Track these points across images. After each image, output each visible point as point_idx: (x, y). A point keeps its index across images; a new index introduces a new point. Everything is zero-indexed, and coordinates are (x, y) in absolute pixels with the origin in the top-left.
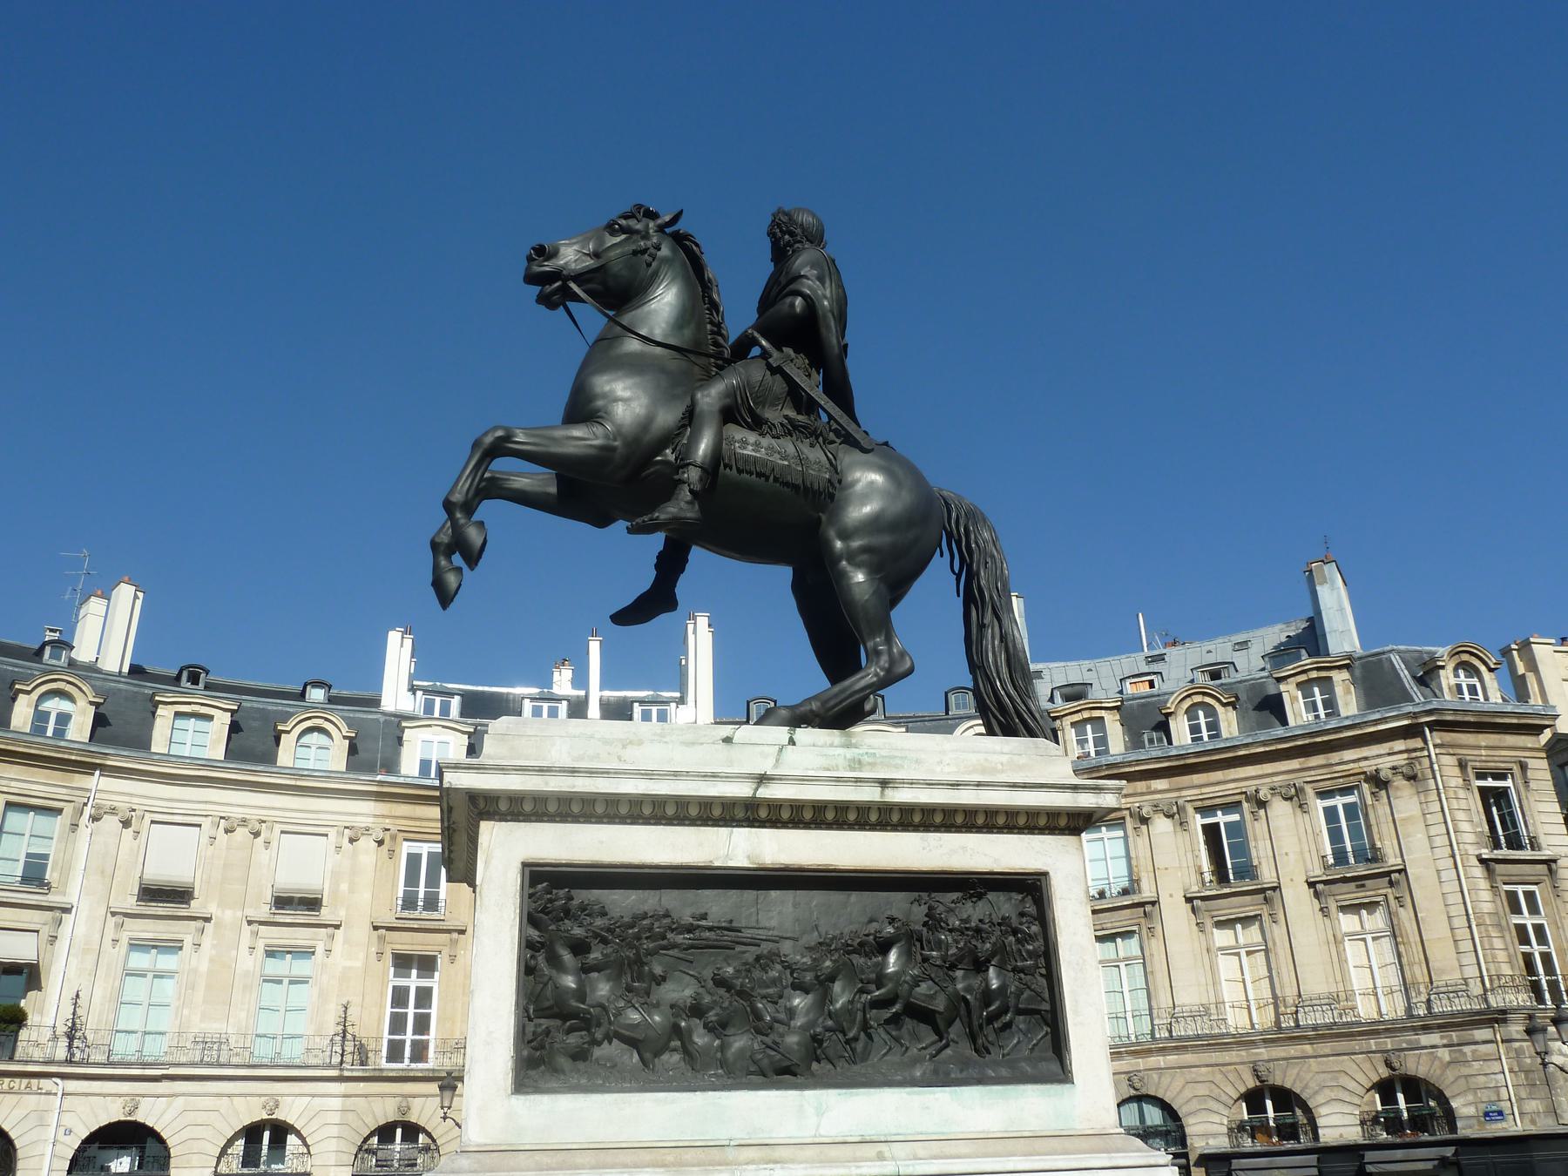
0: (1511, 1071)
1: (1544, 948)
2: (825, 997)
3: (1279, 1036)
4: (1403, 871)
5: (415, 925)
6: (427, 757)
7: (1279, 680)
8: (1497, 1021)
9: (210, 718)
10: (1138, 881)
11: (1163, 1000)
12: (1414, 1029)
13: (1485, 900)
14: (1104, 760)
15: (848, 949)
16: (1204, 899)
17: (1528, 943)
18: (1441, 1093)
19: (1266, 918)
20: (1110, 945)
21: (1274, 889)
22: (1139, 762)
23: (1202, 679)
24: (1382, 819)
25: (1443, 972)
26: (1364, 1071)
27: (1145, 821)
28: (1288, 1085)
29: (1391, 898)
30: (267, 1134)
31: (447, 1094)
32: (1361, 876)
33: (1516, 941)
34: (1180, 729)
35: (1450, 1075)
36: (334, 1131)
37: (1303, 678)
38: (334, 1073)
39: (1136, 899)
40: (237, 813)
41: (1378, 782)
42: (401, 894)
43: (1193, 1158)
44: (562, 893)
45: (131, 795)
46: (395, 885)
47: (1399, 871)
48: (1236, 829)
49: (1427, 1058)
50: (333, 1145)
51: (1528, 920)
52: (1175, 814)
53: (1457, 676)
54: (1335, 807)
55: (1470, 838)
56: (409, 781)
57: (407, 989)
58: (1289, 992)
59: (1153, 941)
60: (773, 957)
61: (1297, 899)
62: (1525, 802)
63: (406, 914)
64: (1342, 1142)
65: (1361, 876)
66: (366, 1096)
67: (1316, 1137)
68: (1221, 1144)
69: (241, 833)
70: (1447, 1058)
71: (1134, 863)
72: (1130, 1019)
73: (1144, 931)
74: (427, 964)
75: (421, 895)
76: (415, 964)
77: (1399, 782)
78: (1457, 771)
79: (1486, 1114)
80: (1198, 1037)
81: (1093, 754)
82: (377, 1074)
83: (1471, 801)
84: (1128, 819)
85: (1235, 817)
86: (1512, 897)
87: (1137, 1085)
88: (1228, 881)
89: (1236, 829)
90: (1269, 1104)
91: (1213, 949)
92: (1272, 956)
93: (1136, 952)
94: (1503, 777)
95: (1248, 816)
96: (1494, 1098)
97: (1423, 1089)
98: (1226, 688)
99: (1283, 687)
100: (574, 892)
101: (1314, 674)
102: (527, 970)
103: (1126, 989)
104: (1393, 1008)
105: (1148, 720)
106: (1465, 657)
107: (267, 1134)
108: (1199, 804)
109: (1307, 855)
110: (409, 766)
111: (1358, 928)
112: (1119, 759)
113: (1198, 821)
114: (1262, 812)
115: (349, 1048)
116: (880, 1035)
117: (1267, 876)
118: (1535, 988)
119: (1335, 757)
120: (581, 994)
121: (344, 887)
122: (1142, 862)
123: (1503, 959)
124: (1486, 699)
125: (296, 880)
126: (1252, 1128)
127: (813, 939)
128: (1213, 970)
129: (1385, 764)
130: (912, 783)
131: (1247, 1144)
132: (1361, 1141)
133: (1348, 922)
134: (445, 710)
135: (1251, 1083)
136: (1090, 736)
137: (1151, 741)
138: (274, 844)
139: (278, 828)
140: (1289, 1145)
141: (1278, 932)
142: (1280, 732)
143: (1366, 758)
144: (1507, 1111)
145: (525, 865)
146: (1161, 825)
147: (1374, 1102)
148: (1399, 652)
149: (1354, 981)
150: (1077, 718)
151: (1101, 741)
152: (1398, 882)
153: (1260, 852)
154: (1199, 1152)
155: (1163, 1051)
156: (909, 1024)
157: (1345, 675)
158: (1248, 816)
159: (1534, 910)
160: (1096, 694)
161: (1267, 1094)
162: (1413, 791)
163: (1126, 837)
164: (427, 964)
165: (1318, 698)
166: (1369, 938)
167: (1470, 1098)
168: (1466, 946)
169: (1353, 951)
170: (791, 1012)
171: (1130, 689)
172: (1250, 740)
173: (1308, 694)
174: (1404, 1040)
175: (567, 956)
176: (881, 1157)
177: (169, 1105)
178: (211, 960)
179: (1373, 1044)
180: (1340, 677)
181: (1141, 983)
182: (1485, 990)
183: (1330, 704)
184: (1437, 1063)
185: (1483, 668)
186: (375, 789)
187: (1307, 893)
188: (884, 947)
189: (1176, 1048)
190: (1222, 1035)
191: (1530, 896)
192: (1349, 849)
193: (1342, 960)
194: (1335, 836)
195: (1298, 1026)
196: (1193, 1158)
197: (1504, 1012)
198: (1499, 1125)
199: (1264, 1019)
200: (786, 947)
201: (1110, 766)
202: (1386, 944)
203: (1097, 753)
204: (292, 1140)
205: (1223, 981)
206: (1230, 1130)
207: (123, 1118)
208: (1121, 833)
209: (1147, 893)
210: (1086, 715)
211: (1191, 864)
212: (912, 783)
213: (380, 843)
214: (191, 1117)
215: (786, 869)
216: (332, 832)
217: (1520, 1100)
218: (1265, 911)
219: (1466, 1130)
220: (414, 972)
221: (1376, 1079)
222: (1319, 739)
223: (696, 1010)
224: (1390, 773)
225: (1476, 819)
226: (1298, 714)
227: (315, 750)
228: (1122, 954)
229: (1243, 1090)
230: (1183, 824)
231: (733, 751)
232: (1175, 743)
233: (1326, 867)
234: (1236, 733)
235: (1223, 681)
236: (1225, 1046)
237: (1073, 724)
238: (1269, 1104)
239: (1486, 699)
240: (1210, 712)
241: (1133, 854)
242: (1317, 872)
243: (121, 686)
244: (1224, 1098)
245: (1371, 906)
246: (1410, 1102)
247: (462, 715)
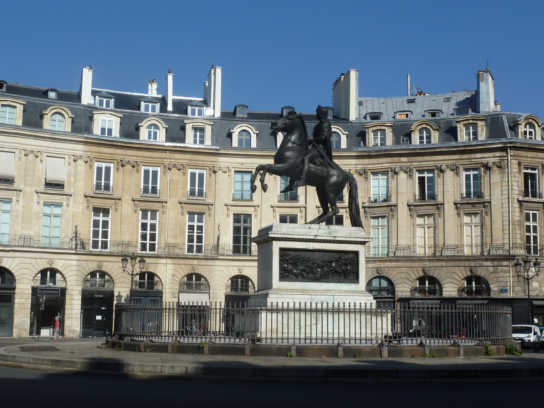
0: (513, 276)
1: (535, 234)
2: (323, 269)
3: (434, 258)
4: (490, 202)
5: (101, 196)
6: (103, 127)
7: (458, 122)
8: (512, 259)
9: (15, 107)
10: (390, 197)
11: (394, 242)
12: (482, 260)
13: (517, 215)
14: (383, 148)
15: (327, 262)
16: (414, 206)
17: (530, 232)
18: (487, 282)
19: (436, 215)
20: (377, 220)
21: (441, 204)
22: (397, 150)
23: (428, 117)
24: (486, 182)
25: (497, 240)
26: (462, 273)
27: (396, 173)
28: (434, 276)
29: (484, 212)
30: (49, 273)
31: (125, 262)
32: (475, 202)
33: (525, 231)
34: (416, 138)
35: (492, 276)
36: (74, 273)
37: (466, 122)
38: (74, 252)
39: (389, 203)
40: (29, 148)
41: (487, 167)
42: (95, 184)
43: (396, 299)
46: (92, 180)
47: (488, 202)
48: (431, 180)
49: (485, 270)
50: (74, 278)
51: (531, 224)
52: (409, 172)
53: (525, 127)
54: (470, 175)
55: (516, 192)
56: (98, 137)
57: (99, 221)
58: (441, 243)
59: (393, 220)
60: (316, 263)
61: (449, 209)
62: (540, 180)
63: (97, 192)
64: (450, 296)
65: (475, 202)
66: (86, 261)
67: (441, 294)
68: (407, 295)
69: (31, 156)
70: (492, 270)
71: (390, 189)
72: (380, 249)
73: (390, 216)
74: (106, 212)
75: (103, 184)
76: (102, 211)
77: (495, 168)
78: (517, 166)
79: (501, 290)
80: (404, 257)
81: (379, 145)
82: (90, 253)
83: (520, 177)
84: (390, 172)
85: (431, 175)
86: (528, 215)
87: (380, 272)
88: (425, 199)
89: (431, 180)
90: (427, 282)
91: (415, 225)
92: (437, 229)
93: (386, 224)
94: (535, 169)
95: (436, 175)
96: (505, 285)
97: (482, 280)
98: (436, 122)
99: (458, 125)
101: (471, 121)
102: (280, 264)
103: (380, 237)
104: (476, 251)
105: (403, 132)
106: (530, 121)
107: (49, 273)
108: (418, 169)
109: (456, 192)
110: (97, 131)
111: (470, 222)
112: (389, 148)
113: (417, 175)
114: (442, 174)
115: (79, 242)
116: (331, 275)
117: (440, 199)
118: (528, 249)
119: (473, 156)
120: (287, 267)
121: (73, 180)
122: (393, 189)
123: (519, 238)
124: (535, 138)
125: (52, 177)
126: (420, 290)
127: (321, 260)
128: (414, 233)
129: (491, 161)
131: (417, 295)
132: (457, 297)
133: (467, 219)
134: (108, 104)
135: (422, 274)
136: (379, 137)
137: (403, 141)
138: (44, 161)
139: (45, 154)
140: (432, 297)
141: (440, 220)
142: (454, 144)
143: (484, 158)
144: (508, 290)
146: (403, 176)
147: (464, 284)
148: (506, 114)
149: (465, 241)
150: (374, 129)
151: (383, 139)
152: (487, 206)
153: (438, 190)
154: (399, 297)
155: (391, 261)
156: (335, 274)
157: (483, 123)
158: (436, 175)
159: (535, 220)
160: (384, 118)
161: (427, 279)
162: (499, 172)
163: (388, 179)
164: (106, 212)
165: (471, 131)
166: (473, 226)
167: (497, 284)
168: (506, 232)
169: (466, 230)
170: (318, 271)
171: (398, 117)
172: (442, 146)
173: (467, 129)
174: (478, 263)
175: (286, 262)
177: (13, 261)
179: (467, 264)
180: (480, 124)
181: (386, 236)
182: (510, 248)
183: (475, 134)
184: (488, 272)
185: (536, 125)
186: (84, 140)
187: (453, 206)
188: (332, 262)
189: (396, 260)
190: (413, 257)
191: (534, 215)
192: (472, 192)
193: (462, 233)
194: (468, 186)
195: (441, 255)
196: (396, 299)
197: (514, 256)
198: (505, 294)
199: (429, 252)
200: (317, 261)
201: (385, 150)
202: (479, 228)
203: (381, 144)
204: (58, 276)
205: (416, 237)
206: (411, 290)
208: (386, 177)
209: (393, 201)
210: (378, 128)
211: (412, 192)
213: (86, 162)
214: (22, 266)
216: (67, 157)
217: (513, 286)
218: (437, 212)
219: (493, 295)
220: (101, 214)
221: (466, 276)
222: (468, 148)
223: (304, 270)
224: (492, 164)
225: (520, 185)
226: (463, 136)
227: (57, 121)
228: (380, 224)
229: (418, 276)
230: (411, 176)
231: (311, 230)
232: (413, 143)
233: (462, 198)
234: (437, 142)
235: (436, 118)
236: (414, 261)
237: (373, 131)
238: (427, 282)
239: (535, 138)
240: (428, 131)
241: (390, 186)
242: (459, 199)
244: (411, 279)
245: (476, 214)
246: (477, 285)
247: (115, 107)
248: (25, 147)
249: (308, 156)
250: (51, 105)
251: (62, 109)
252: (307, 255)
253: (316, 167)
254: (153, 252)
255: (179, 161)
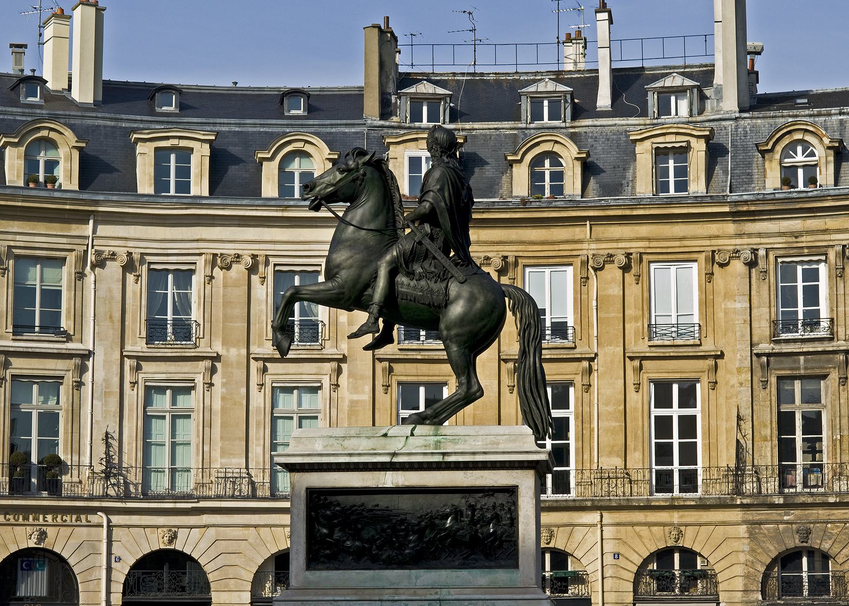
44: (322, 498)
45: (126, 239)
100: (328, 497)
130: (456, 453)
145: (307, 489)
176: (436, 593)
178: (223, 398)
207: (162, 547)
212: (456, 453)
214: (222, 546)
215: (408, 487)
231: (388, 440)
243: (101, 122)
248: (219, 248)
249: (388, 257)
250: (285, 135)
251: (307, 142)
252: (383, 501)
253: (413, 283)
254: (565, 497)
255: (621, 245)
